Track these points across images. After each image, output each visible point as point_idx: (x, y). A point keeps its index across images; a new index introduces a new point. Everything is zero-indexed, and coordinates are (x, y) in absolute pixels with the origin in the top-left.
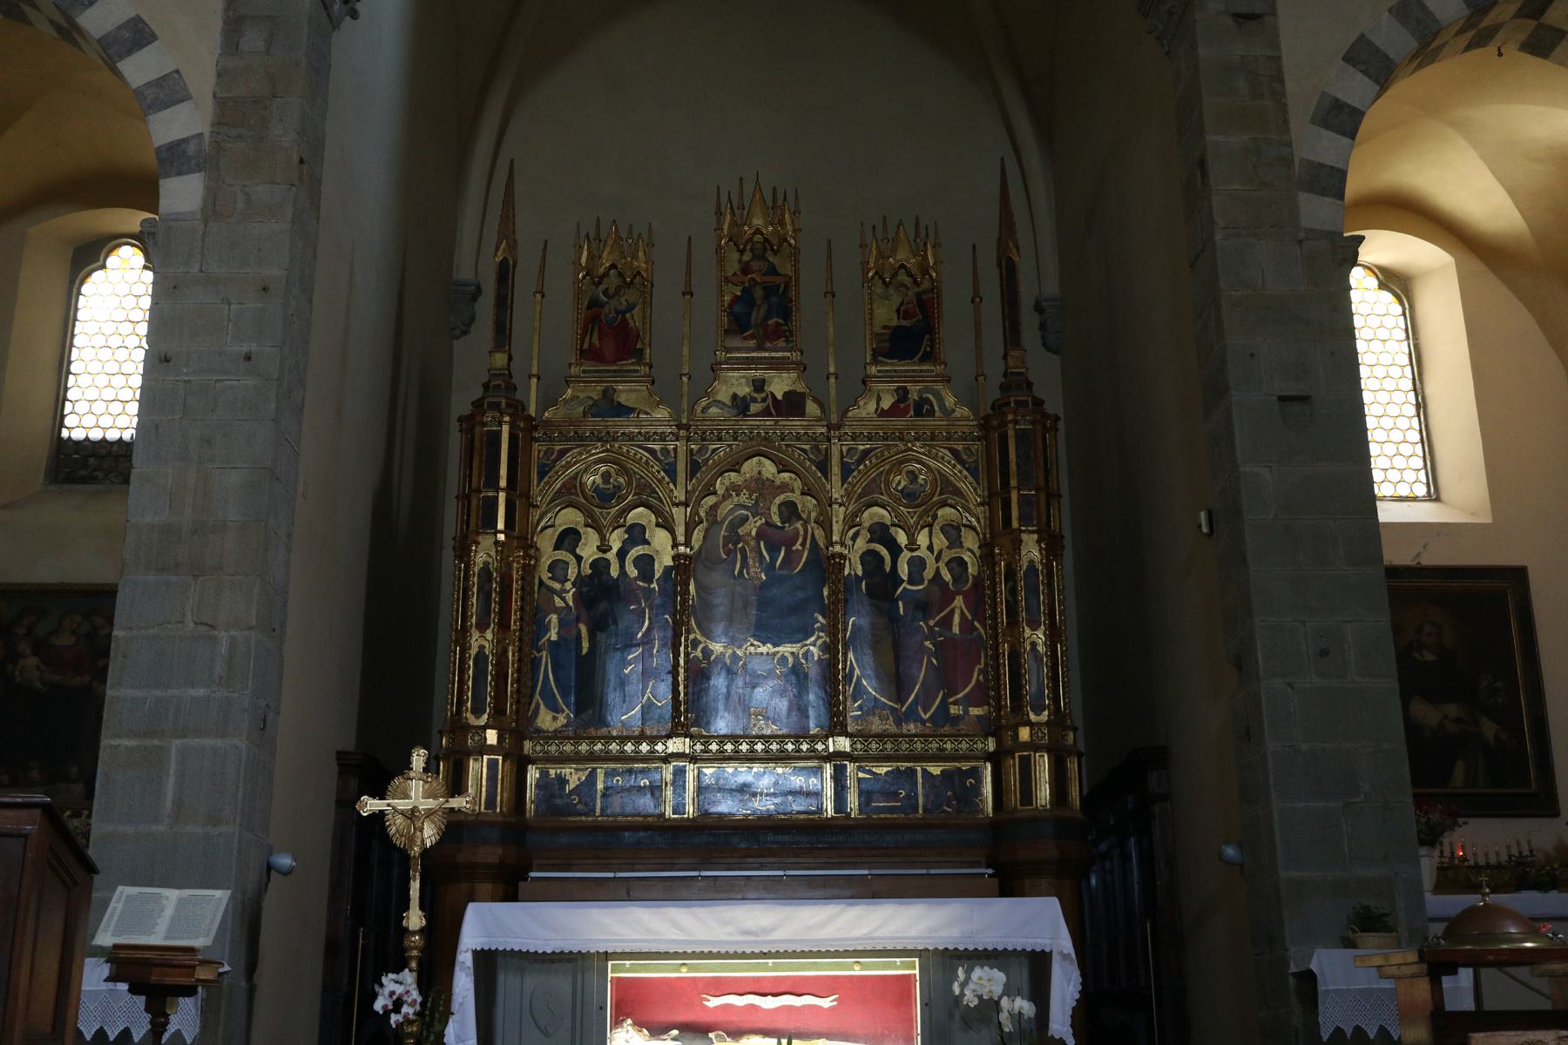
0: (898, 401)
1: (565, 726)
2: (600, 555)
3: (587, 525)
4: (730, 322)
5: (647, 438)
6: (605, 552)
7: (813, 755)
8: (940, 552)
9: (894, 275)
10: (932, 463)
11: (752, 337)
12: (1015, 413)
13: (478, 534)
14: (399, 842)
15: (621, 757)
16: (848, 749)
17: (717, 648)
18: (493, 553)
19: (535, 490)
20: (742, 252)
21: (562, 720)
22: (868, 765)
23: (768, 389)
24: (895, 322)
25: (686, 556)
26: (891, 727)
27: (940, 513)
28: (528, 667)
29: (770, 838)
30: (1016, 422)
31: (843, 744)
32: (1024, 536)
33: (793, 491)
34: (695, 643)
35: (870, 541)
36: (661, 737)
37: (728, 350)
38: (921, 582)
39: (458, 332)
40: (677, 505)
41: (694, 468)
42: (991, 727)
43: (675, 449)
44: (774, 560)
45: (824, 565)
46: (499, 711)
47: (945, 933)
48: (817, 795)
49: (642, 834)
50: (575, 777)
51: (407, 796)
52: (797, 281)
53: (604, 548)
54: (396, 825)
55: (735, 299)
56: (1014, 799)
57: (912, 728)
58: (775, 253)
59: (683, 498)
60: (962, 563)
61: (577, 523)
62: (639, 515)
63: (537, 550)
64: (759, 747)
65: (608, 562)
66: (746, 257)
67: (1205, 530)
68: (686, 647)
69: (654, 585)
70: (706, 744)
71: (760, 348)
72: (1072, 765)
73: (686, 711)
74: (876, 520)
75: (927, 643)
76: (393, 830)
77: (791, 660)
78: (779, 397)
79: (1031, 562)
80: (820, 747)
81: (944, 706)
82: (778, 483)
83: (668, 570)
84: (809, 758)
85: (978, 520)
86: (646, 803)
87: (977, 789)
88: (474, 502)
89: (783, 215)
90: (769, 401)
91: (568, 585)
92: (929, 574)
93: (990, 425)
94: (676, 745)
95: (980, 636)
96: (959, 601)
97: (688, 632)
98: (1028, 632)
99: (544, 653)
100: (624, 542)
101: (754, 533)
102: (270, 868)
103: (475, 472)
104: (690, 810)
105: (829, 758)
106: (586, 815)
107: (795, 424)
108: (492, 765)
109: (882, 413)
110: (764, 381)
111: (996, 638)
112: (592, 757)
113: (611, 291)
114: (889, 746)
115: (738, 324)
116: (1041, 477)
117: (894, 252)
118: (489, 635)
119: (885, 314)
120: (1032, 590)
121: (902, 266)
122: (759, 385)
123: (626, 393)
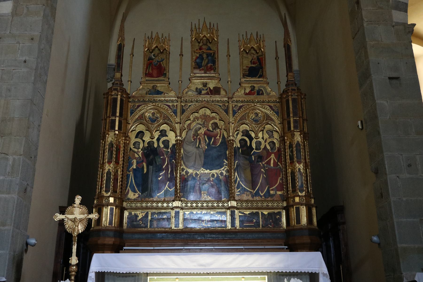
0: (251, 90)
1: (139, 197)
2: (151, 140)
3: (146, 130)
4: (195, 65)
5: (167, 101)
6: (152, 139)
7: (223, 207)
8: (266, 139)
9: (250, 50)
10: (263, 110)
11: (203, 70)
12: (291, 92)
13: (109, 131)
14: (69, 231)
15: (157, 208)
16: (236, 205)
17: (190, 171)
18: (114, 138)
19: (129, 118)
20: (199, 43)
21: (137, 195)
22: (242, 211)
23: (208, 86)
24: (250, 65)
25: (180, 140)
26: (250, 198)
27: (266, 126)
28: (125, 177)
29: (209, 236)
30: (292, 96)
32: (295, 133)
33: (216, 119)
34: (183, 169)
35: (242, 136)
36: (171, 201)
37: (195, 74)
38: (260, 149)
39: (109, 80)
40: (177, 123)
41: (183, 111)
42: (285, 198)
43: (177, 105)
44: (210, 142)
45: (226, 143)
46: (115, 191)
47: (278, 266)
48: (225, 221)
49: (164, 234)
50: (141, 215)
51: (72, 213)
52: (217, 52)
53: (152, 137)
54: (68, 225)
55: (197, 58)
56: (294, 222)
57: (257, 198)
58: (210, 43)
59: (179, 121)
60: (274, 143)
61: (143, 129)
62: (164, 127)
63: (129, 138)
65: (154, 142)
66: (200, 45)
67: (360, 127)
68: (180, 171)
69: (169, 150)
71: (205, 73)
72: (314, 211)
73: (180, 192)
74: (244, 129)
76: (67, 226)
77: (216, 175)
78: (212, 89)
79: (298, 142)
80: (226, 205)
81: (268, 191)
82: (211, 116)
83: (174, 145)
84: (222, 208)
85: (279, 129)
86: (165, 224)
87: (280, 219)
88: (108, 121)
89: (213, 31)
90: (208, 90)
91: (140, 150)
92: (262, 147)
93: (283, 97)
94: (177, 204)
95: (280, 168)
96: (273, 156)
97: (181, 166)
98: (297, 165)
99: (131, 173)
100: (159, 136)
101: (203, 133)
102: (27, 244)
103: (108, 111)
104: (181, 226)
105: (229, 208)
106: (145, 228)
107: (217, 98)
108: (112, 210)
109: (246, 94)
110: (206, 83)
111: (286, 168)
112: (147, 208)
113: (156, 55)
114: (249, 204)
115: (198, 66)
116: (301, 113)
117: (250, 42)
118: (112, 165)
119: (247, 63)
120: (298, 151)
121: (252, 47)
122: (205, 85)
123: (160, 86)
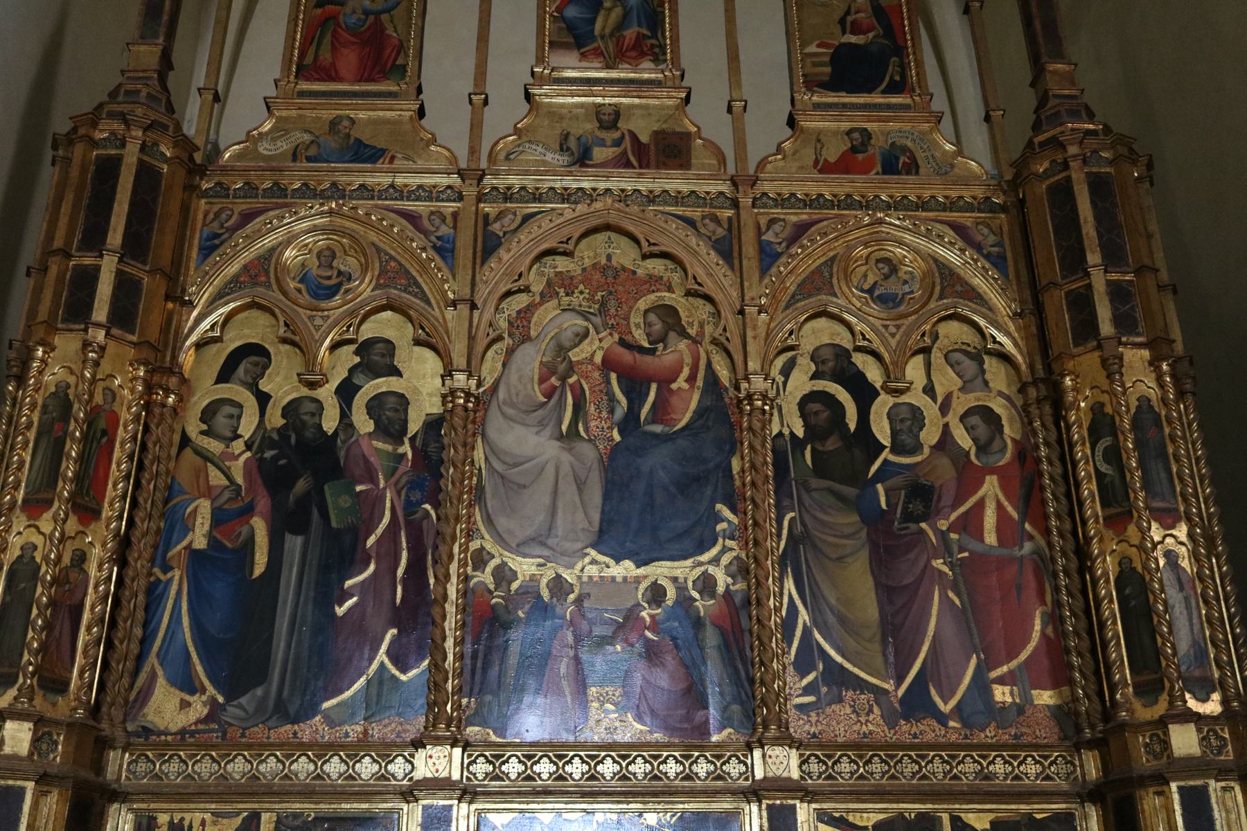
0: (854, 150)
2: (305, 391)
6: (312, 385)
8: (948, 398)
17: (524, 567)
21: (198, 708)
31: (784, 762)
33: (670, 289)
34: (480, 559)
35: (815, 376)
36: (404, 746)
38: (917, 448)
62: (385, 325)
64: (608, 768)
69: (406, 449)
70: (497, 759)
73: (459, 691)
75: (938, 563)
78: (644, 138)
79: (1144, 401)
80: (734, 768)
81: (981, 685)
90: (627, 142)
91: (238, 446)
92: (930, 436)
94: (438, 761)
96: (991, 486)
97: (470, 535)
98: (1156, 533)
99: (177, 574)
101: (598, 359)
105: (755, 792)
114: (877, 767)
